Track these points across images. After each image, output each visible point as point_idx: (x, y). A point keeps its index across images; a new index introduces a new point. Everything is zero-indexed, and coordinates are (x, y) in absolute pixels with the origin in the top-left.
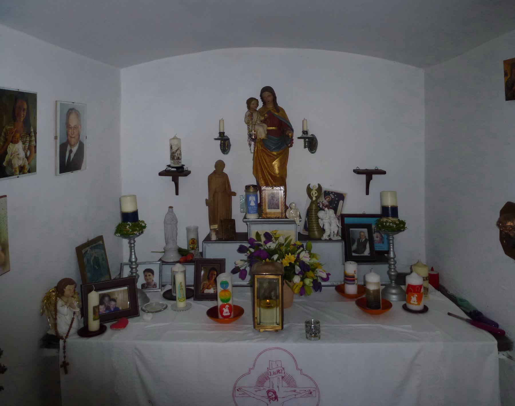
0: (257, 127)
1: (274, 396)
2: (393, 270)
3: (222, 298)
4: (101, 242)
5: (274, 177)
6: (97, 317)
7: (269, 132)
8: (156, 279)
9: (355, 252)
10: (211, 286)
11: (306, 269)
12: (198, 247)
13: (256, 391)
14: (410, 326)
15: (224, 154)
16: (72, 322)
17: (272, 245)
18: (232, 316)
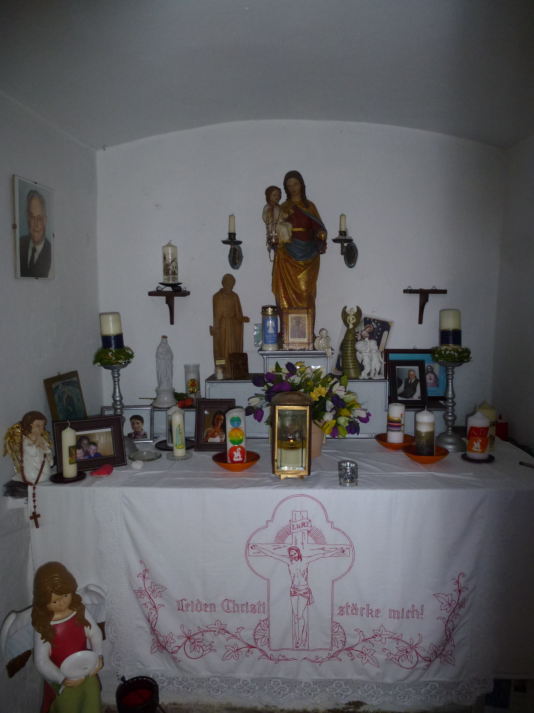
0: (278, 227)
1: (297, 555)
2: (450, 414)
3: (233, 439)
4: (75, 379)
5: (299, 296)
6: (74, 461)
7: (295, 235)
8: (146, 427)
9: (401, 395)
10: (216, 433)
11: (340, 404)
12: (199, 389)
13: (275, 549)
14: (472, 474)
15: (234, 268)
16: (42, 467)
17: (296, 379)
18: (245, 461)
